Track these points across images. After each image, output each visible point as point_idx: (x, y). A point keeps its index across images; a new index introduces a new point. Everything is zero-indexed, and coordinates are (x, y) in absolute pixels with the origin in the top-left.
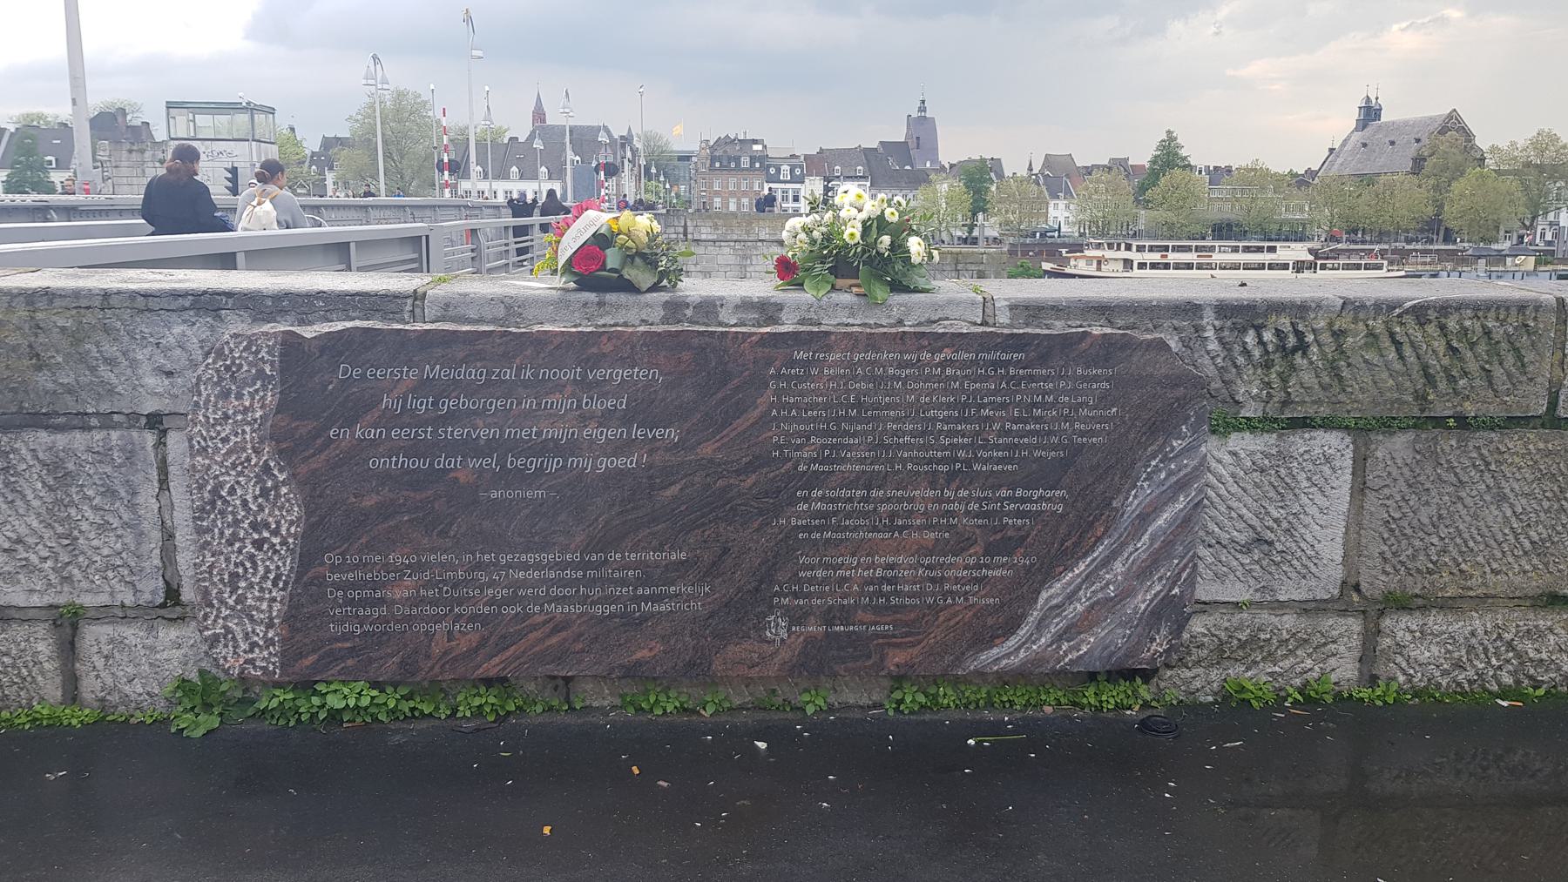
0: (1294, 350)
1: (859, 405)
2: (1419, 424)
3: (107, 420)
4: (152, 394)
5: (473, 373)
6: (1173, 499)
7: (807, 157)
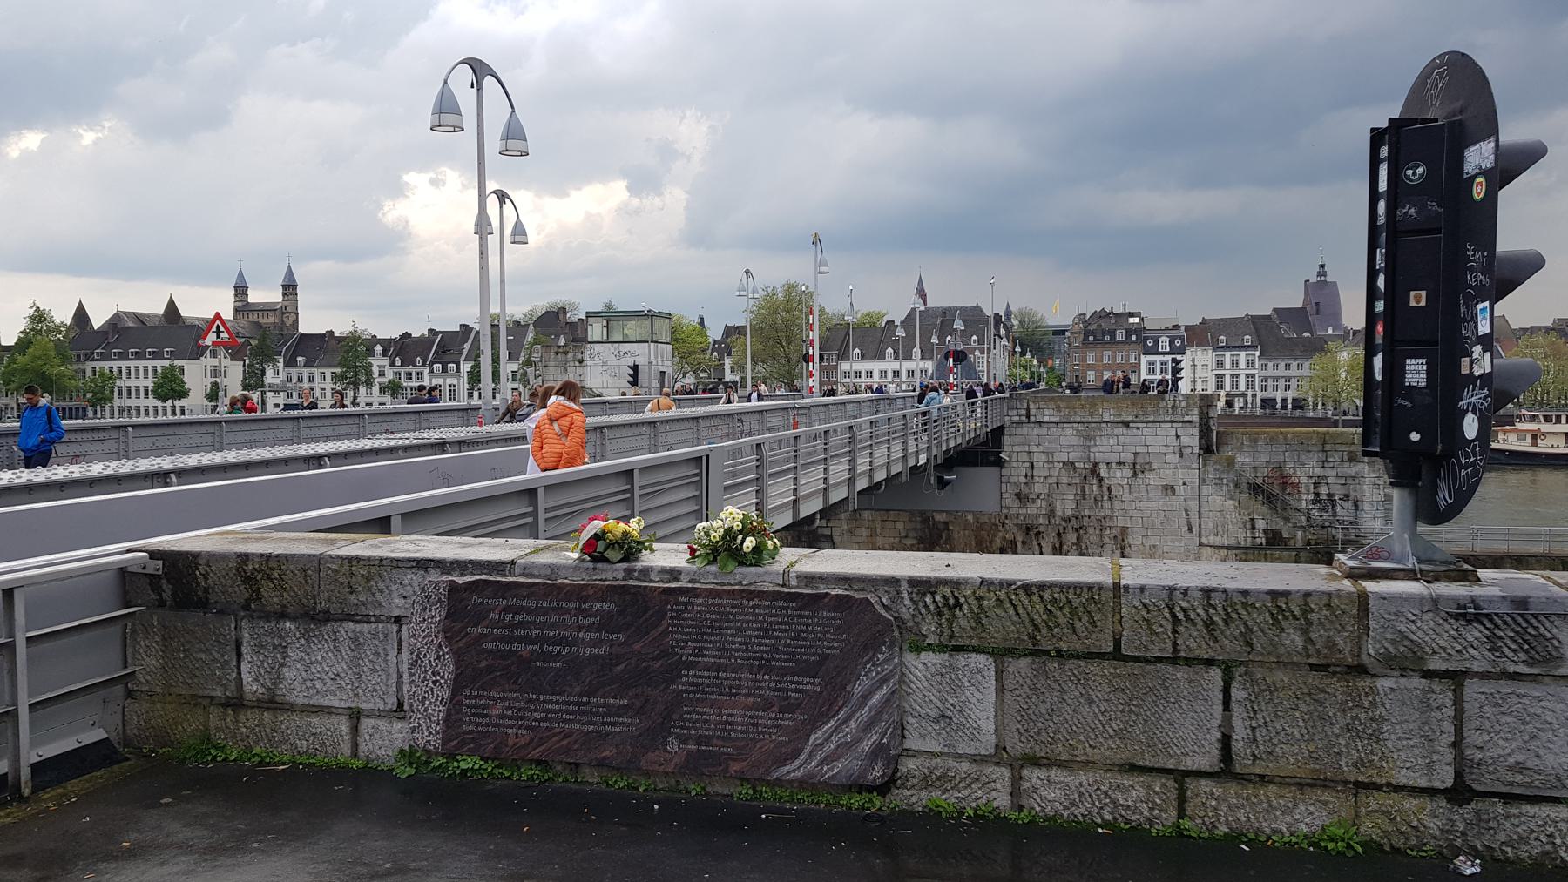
0: (955, 607)
1: (712, 627)
2: (1036, 653)
3: (378, 620)
4: (397, 607)
5: (531, 603)
6: (880, 687)
7: (1188, 328)
